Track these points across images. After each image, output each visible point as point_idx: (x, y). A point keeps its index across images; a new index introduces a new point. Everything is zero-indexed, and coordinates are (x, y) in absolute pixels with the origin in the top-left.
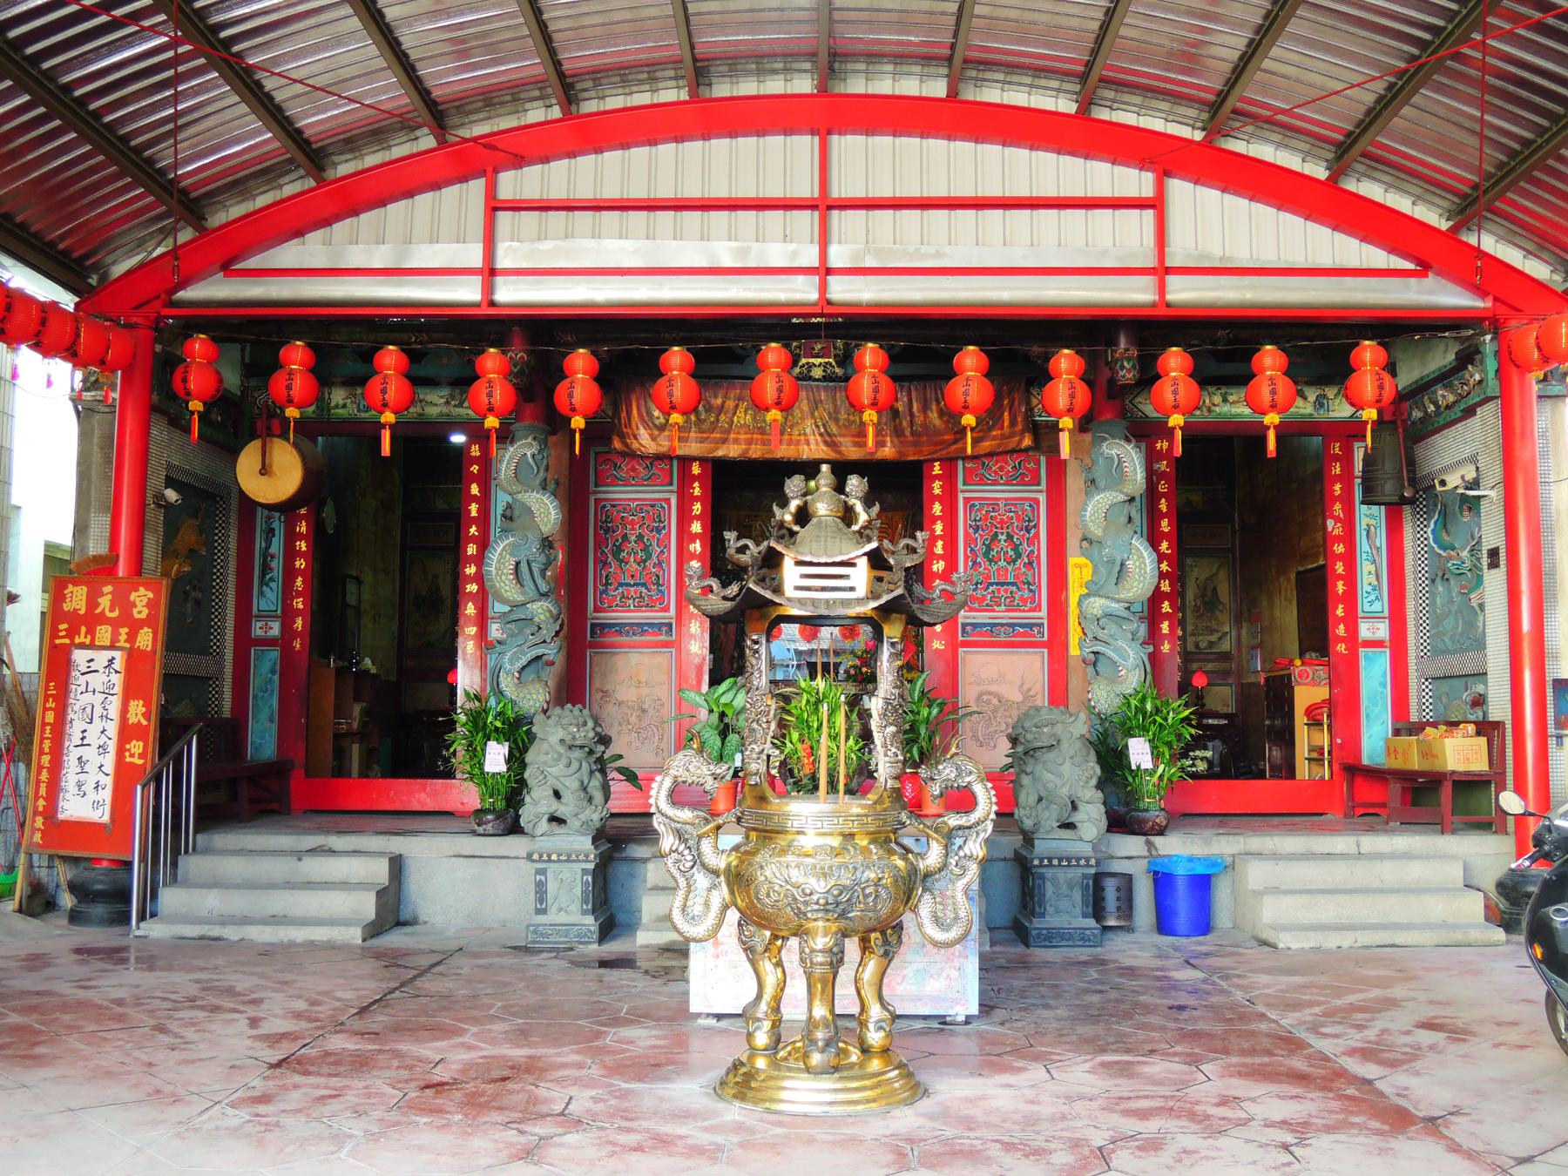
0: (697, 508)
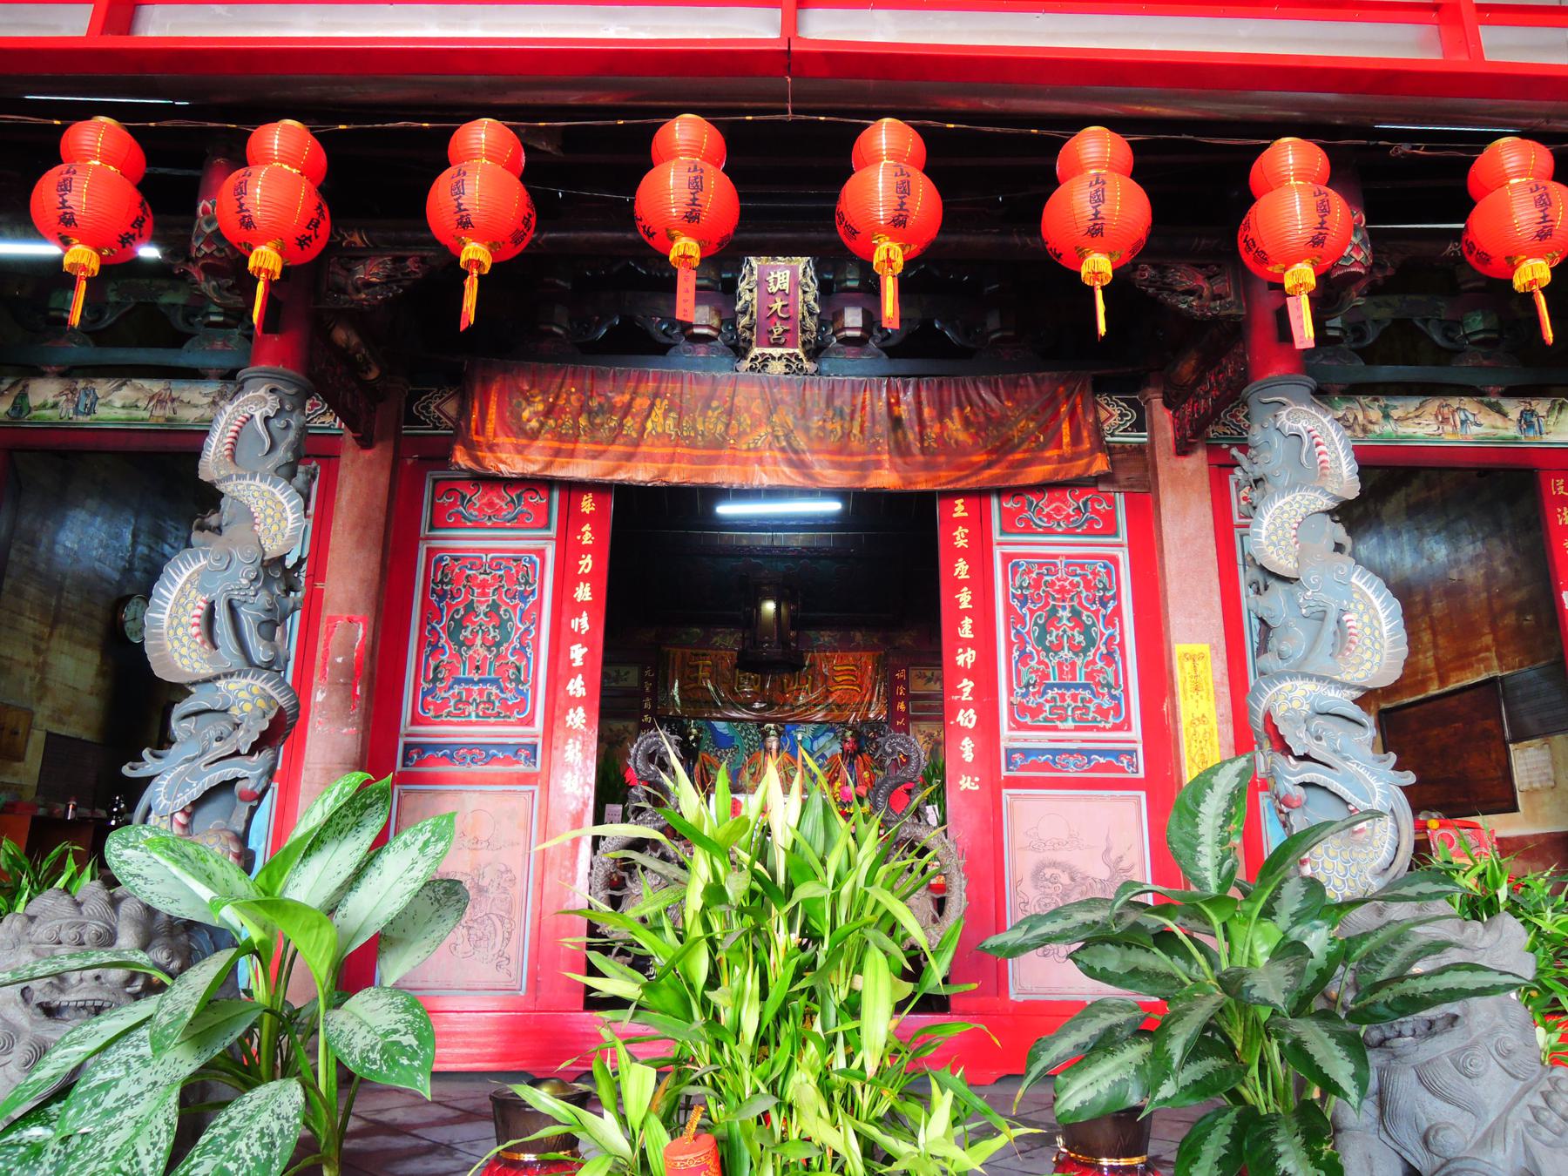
0: (586, 563)
